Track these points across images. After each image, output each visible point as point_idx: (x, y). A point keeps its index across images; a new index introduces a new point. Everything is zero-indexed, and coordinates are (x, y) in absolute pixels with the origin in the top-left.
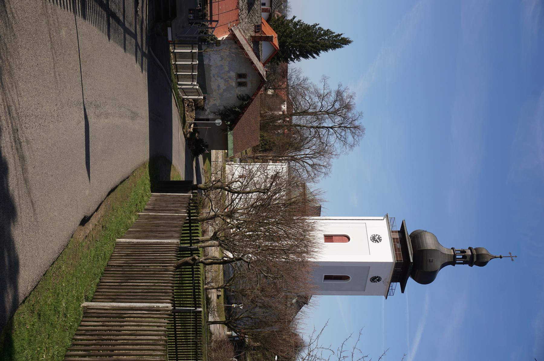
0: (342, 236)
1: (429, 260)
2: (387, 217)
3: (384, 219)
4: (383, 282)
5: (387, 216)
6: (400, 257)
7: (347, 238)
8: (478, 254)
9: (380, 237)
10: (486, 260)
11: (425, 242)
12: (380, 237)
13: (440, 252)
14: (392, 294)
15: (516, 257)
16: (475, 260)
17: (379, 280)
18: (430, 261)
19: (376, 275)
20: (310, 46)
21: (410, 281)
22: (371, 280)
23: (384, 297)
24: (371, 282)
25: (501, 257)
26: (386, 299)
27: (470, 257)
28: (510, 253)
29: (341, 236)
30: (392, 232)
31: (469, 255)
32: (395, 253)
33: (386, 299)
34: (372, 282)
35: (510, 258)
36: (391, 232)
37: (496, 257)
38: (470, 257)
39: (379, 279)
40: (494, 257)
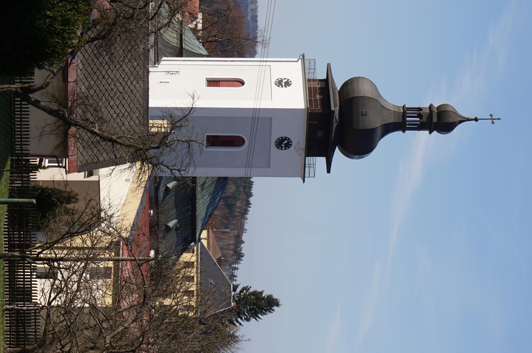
0: (233, 81)
1: (361, 113)
2: (303, 59)
3: (298, 60)
4: (295, 148)
5: (303, 56)
6: (316, 106)
7: (242, 83)
8: (439, 111)
9: (289, 81)
10: (451, 120)
11: (356, 90)
12: (289, 81)
13: (379, 105)
14: (312, 174)
15: (499, 119)
16: (435, 120)
17: (288, 145)
18: (363, 114)
19: (284, 135)
20: (196, 344)
21: (338, 154)
22: (276, 145)
23: (300, 179)
24: (277, 149)
25: (476, 120)
26: (304, 182)
27: (427, 116)
28: (491, 115)
29: (232, 81)
30: (309, 80)
31: (427, 113)
32: (308, 98)
33: (304, 182)
34: (278, 148)
35: (491, 120)
36: (308, 81)
37: (468, 120)
38: (428, 116)
39: (288, 142)
40: (466, 119)
